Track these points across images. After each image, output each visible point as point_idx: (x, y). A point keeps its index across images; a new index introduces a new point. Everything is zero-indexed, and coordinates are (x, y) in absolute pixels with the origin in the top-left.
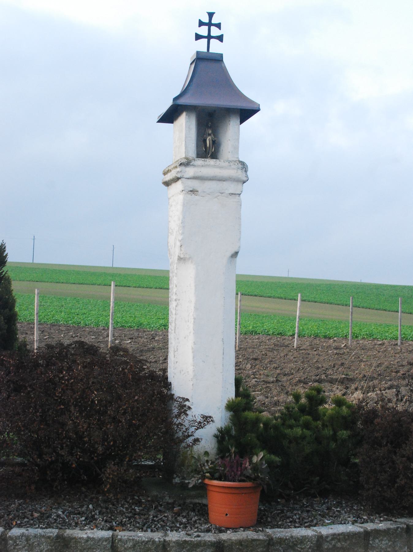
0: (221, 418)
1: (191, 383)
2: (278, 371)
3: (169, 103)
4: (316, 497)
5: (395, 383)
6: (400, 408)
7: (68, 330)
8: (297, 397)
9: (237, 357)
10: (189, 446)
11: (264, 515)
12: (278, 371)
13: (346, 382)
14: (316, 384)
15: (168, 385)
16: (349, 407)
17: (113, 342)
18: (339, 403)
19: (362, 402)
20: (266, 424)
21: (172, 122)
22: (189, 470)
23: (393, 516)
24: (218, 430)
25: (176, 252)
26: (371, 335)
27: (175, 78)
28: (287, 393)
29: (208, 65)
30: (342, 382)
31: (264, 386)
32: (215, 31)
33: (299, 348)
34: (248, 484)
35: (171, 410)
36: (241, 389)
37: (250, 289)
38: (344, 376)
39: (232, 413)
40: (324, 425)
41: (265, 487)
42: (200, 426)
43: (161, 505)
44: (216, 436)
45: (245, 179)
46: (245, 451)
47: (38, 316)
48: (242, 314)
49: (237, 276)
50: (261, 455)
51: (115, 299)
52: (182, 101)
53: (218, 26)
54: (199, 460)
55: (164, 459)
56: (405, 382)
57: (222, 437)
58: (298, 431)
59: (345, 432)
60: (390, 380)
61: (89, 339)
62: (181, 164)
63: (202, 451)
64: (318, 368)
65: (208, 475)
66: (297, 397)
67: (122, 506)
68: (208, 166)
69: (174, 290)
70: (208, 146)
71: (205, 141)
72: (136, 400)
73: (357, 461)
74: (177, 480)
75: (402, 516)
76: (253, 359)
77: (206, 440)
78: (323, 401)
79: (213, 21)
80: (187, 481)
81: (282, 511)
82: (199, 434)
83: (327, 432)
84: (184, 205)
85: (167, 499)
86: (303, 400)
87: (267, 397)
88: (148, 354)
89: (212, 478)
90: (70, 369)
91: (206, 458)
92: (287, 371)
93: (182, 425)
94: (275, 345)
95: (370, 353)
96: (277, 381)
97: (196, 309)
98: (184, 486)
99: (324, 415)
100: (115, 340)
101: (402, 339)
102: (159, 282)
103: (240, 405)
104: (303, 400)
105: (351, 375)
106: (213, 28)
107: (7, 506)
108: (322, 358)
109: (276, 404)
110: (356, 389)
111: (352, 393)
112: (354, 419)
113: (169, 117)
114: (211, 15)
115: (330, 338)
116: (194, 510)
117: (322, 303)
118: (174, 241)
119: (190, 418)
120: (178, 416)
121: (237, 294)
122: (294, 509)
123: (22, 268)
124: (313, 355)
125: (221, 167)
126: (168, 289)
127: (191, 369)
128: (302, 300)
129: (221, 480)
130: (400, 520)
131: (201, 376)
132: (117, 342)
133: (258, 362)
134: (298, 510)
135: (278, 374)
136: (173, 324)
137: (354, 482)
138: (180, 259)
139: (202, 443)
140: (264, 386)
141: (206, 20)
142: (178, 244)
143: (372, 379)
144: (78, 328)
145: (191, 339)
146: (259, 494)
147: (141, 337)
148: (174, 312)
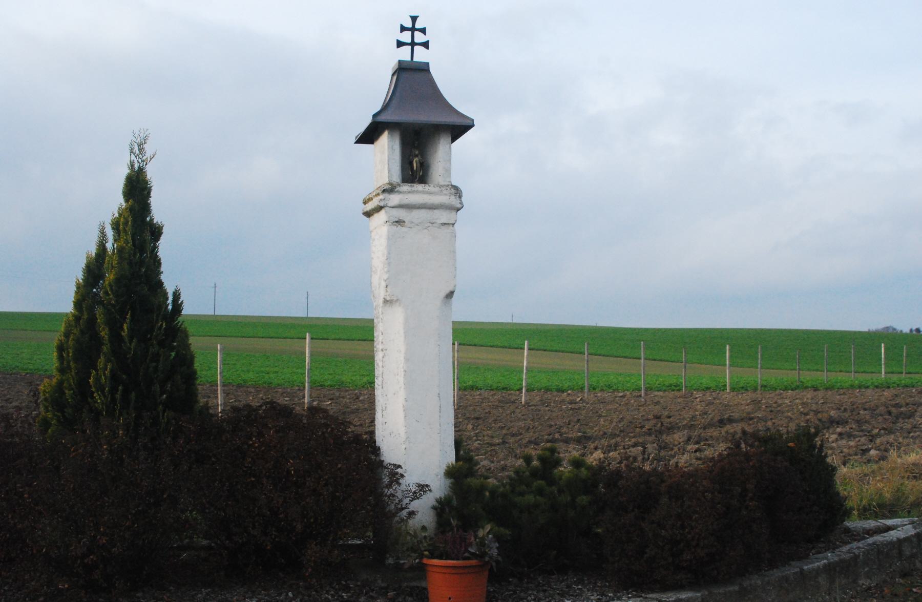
0: (439, 487)
1: (404, 446)
2: (504, 432)
3: (366, 121)
4: (554, 574)
5: (640, 440)
6: (647, 467)
7: (258, 392)
8: (528, 459)
9: (456, 417)
10: (402, 520)
11: (494, 597)
12: (504, 432)
13: (583, 440)
14: (549, 445)
15: (376, 450)
16: (589, 468)
17: (309, 403)
18: (577, 464)
19: (604, 462)
20: (493, 492)
21: (372, 143)
22: (405, 549)
23: (643, 592)
24: (437, 500)
25: (381, 294)
26: (610, 387)
27: (373, 92)
28: (516, 456)
29: (412, 77)
30: (578, 441)
31: (489, 449)
32: (419, 37)
33: (527, 403)
34: (474, 562)
35: (381, 479)
36: (462, 452)
37: (467, 337)
38: (579, 434)
39: (452, 480)
40: (561, 491)
41: (494, 564)
42: (415, 496)
43: (373, 590)
44: (434, 508)
45: (459, 206)
46: (469, 523)
47: (222, 376)
48: (461, 367)
49: (454, 323)
50: (488, 527)
51: (311, 355)
52: (383, 118)
53: (423, 31)
54: (415, 536)
55: (374, 537)
56: (650, 439)
57: (441, 508)
58: (530, 498)
59: (584, 497)
60: (634, 437)
61: (284, 401)
62: (384, 191)
63: (418, 526)
64: (551, 426)
65: (426, 553)
66: (528, 459)
67: (327, 592)
68: (417, 192)
69: (380, 338)
70: (415, 170)
71: (411, 163)
72: (339, 469)
73: (599, 530)
74: (390, 561)
75: (653, 591)
76: (474, 418)
77: (422, 512)
78: (558, 463)
79: (417, 26)
80: (402, 562)
81: (515, 592)
82: (415, 505)
83: (565, 498)
84: (389, 239)
85: (380, 583)
86: (535, 463)
87: (493, 462)
88: (352, 416)
89: (432, 556)
90: (260, 434)
91: (423, 534)
92: (514, 430)
93: (394, 496)
94: (500, 401)
95: (610, 407)
96: (504, 442)
97: (407, 360)
98: (398, 567)
99: (561, 479)
100: (313, 401)
101: (646, 389)
102: (361, 333)
103: (461, 472)
104: (535, 463)
105: (590, 432)
106: (416, 33)
107: (193, 596)
108: (554, 414)
109: (504, 468)
110: (596, 448)
111: (592, 454)
112: (592, 481)
113: (369, 136)
114: (414, 19)
115: (563, 392)
116: (411, 595)
117: (552, 351)
118: (378, 280)
119: (403, 487)
120: (389, 486)
121: (454, 344)
122: (528, 589)
123: (200, 320)
124: (545, 411)
125: (431, 193)
126: (373, 341)
127: (402, 430)
128: (529, 349)
129: (441, 558)
130: (650, 596)
131: (414, 431)
132: (315, 403)
133: (481, 422)
134: (532, 590)
135: (506, 434)
136: (380, 379)
137: (606, 596)
138: (386, 301)
139: (418, 517)
140: (489, 449)
141: (409, 24)
142: (383, 284)
143: (614, 436)
144: (269, 387)
145: (402, 394)
146: (486, 573)
147: (343, 397)
148: (380, 364)
